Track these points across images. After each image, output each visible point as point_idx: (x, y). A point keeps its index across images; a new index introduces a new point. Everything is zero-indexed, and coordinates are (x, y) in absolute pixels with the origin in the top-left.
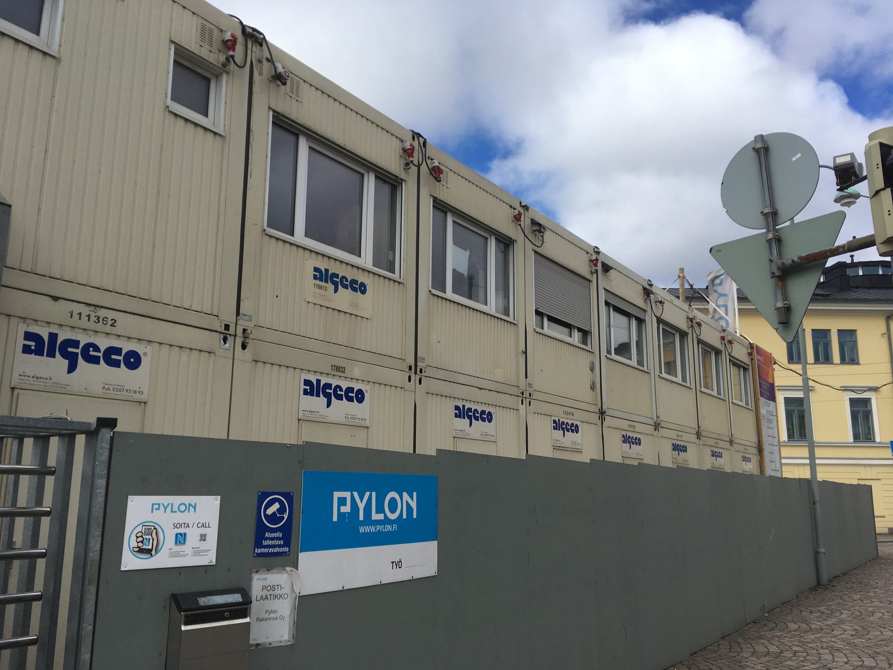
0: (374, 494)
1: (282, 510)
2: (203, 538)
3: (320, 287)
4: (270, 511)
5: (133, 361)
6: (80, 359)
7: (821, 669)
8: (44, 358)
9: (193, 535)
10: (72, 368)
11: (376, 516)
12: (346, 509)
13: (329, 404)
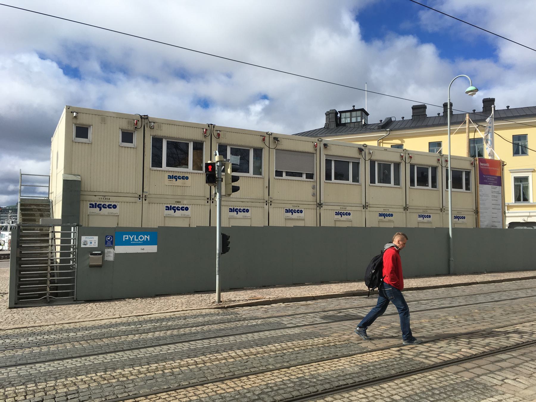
0: (135, 236)
1: (111, 238)
2: (95, 243)
3: (171, 181)
4: (108, 239)
5: (115, 207)
6: (176, 210)
7: (364, 400)
8: (233, 212)
9: (93, 242)
10: (100, 210)
11: (135, 240)
12: (128, 238)
13: (292, 214)
